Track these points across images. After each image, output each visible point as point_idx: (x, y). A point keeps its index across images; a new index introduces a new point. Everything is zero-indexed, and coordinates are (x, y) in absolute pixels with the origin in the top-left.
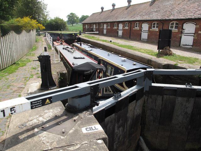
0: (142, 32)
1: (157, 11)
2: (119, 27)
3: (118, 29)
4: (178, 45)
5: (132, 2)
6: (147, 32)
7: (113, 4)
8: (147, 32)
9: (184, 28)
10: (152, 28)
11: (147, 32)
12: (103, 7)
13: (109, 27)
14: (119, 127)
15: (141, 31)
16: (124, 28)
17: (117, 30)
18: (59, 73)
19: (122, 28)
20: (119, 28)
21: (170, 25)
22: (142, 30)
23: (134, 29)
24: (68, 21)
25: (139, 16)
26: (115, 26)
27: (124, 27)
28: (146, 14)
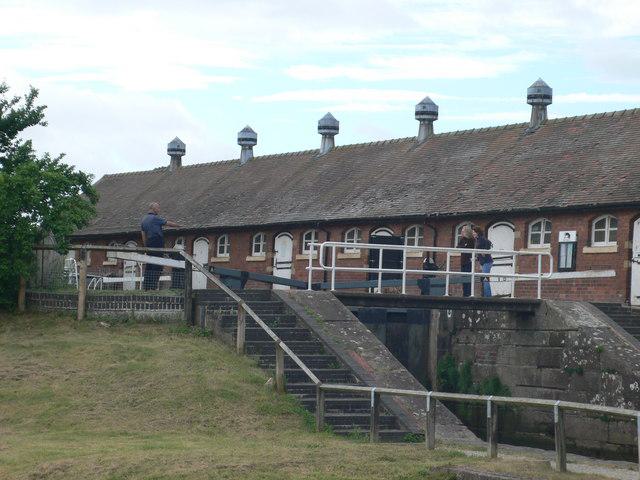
0: (634, 266)
1: (421, 186)
2: (274, 252)
3: (271, 262)
4: (542, 364)
5: (555, 98)
6: (289, 265)
7: (247, 130)
8: (289, 265)
9: (276, 249)
10: (219, 255)
11: (279, 266)
12: (435, 99)
13: (225, 256)
14: (106, 259)
15: (122, 268)
16: (298, 257)
17: (269, 269)
18: (22, 307)
19: (288, 258)
20: (278, 257)
21: (594, 230)
22: (635, 255)
23: (248, 259)
24: (192, 291)
25: (361, 203)
26: (257, 250)
27: (212, 253)
28: (388, 195)
